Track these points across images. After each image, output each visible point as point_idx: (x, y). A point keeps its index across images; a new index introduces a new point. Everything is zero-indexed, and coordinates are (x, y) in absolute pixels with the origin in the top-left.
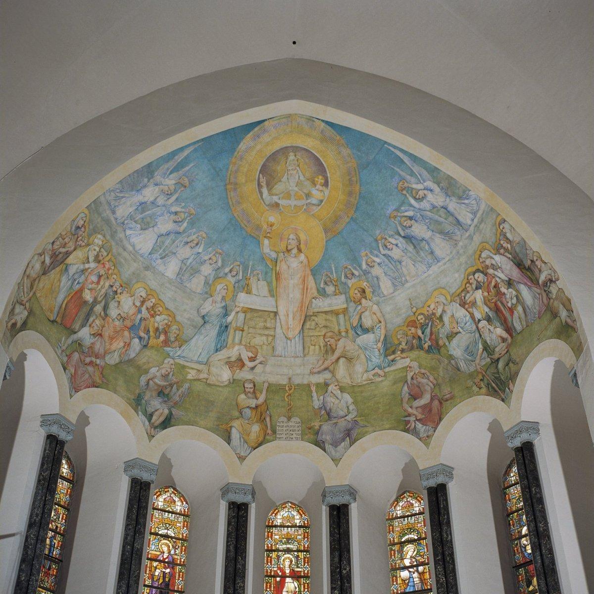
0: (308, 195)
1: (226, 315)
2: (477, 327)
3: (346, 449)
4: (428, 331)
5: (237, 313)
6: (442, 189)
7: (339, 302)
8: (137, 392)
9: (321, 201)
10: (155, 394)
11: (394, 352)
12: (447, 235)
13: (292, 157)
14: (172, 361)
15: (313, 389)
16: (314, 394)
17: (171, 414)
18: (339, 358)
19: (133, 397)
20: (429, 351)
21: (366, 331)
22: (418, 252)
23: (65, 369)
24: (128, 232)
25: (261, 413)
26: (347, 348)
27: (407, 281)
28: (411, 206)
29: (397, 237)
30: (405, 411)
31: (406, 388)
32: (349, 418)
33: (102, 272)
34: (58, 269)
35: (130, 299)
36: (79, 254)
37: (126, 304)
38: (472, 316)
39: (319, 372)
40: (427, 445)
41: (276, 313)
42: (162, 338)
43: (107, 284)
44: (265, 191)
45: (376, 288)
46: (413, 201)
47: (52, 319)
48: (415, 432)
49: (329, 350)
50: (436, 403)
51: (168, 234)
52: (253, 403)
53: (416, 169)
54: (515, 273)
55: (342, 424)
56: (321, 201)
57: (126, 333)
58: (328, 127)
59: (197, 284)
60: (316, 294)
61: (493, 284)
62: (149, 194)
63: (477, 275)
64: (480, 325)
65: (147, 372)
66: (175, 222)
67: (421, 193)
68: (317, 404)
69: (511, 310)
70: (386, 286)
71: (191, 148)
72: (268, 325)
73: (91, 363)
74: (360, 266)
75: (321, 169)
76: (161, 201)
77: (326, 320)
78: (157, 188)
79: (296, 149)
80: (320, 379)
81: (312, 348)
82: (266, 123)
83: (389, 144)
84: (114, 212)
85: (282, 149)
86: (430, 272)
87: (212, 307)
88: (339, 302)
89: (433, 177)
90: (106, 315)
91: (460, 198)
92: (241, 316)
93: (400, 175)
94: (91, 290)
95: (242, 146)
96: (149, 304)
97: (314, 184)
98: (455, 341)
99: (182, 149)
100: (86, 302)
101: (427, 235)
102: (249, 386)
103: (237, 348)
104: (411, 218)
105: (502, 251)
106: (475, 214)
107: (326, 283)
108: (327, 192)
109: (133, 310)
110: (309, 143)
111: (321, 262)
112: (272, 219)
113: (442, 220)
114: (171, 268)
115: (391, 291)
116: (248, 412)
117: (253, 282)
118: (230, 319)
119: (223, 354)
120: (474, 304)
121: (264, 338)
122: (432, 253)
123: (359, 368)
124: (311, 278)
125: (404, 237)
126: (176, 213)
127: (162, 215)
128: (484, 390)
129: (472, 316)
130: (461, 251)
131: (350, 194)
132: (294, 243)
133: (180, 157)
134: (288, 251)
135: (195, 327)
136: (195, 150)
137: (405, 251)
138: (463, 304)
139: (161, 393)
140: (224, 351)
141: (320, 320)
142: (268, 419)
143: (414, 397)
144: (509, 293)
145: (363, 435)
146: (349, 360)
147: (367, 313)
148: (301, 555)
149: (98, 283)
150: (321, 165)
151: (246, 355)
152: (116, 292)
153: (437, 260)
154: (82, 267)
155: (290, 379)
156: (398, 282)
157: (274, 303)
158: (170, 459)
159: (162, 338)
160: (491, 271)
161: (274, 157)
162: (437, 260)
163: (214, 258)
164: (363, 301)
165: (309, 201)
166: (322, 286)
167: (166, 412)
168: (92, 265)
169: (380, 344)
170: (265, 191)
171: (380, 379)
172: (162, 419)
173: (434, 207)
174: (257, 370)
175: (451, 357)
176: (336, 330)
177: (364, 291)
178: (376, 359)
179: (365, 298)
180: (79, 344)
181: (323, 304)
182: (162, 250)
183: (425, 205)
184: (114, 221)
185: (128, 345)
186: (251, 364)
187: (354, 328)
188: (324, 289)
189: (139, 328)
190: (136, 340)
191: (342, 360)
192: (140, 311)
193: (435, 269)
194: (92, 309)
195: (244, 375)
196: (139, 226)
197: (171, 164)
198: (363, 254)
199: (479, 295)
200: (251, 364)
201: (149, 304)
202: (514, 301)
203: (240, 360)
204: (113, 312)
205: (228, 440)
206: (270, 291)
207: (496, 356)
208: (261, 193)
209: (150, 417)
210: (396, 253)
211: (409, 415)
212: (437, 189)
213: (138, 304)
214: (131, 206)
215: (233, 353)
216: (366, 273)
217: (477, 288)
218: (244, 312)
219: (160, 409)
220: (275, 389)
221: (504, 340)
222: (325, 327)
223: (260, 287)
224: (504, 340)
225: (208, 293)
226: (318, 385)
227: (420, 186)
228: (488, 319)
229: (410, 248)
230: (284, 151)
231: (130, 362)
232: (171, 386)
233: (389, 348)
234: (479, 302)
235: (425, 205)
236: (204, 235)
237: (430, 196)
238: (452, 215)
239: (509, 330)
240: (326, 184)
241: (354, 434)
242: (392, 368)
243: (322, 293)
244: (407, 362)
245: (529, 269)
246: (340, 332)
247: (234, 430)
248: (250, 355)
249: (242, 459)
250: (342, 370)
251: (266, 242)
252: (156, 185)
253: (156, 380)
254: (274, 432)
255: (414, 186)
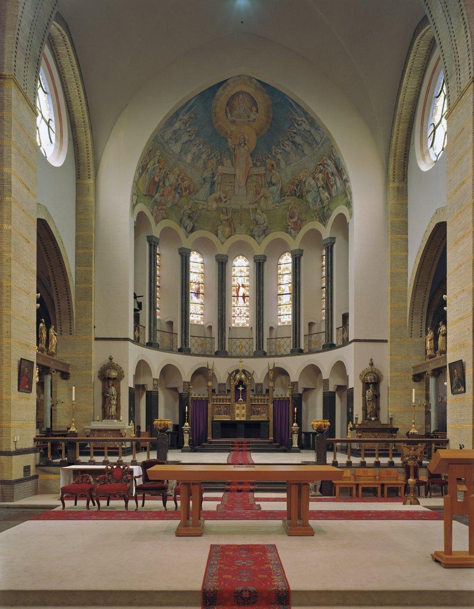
0: (249, 117)
1: (213, 177)
2: (318, 190)
3: (263, 239)
4: (299, 188)
5: (218, 176)
6: (309, 122)
7: (262, 170)
8: (180, 218)
9: (255, 120)
10: (187, 217)
11: (284, 196)
12: (310, 145)
13: (241, 96)
14: (192, 202)
15: (251, 211)
16: (251, 213)
17: (194, 225)
18: (261, 198)
19: (178, 220)
20: (299, 197)
21: (273, 185)
22: (297, 150)
23: (152, 214)
24: (170, 145)
25: (230, 223)
26: (265, 192)
27: (291, 163)
28: (295, 127)
29: (288, 141)
30: (287, 223)
31: (288, 213)
32: (265, 224)
33: (161, 167)
34: (145, 172)
35: (173, 176)
36: (152, 162)
37: (172, 178)
38: (317, 185)
39: (253, 203)
40: (294, 240)
41: (235, 175)
42: (188, 191)
43: (164, 171)
44: (229, 115)
45: (278, 165)
46: (296, 125)
47: (145, 194)
48: (290, 233)
49: (257, 193)
50: (299, 221)
51: (187, 142)
52: (226, 218)
53: (298, 110)
54: (335, 171)
55: (262, 227)
56: (255, 120)
57: (173, 192)
58: (259, 83)
59: (200, 164)
60: (252, 166)
61: (326, 172)
62: (177, 125)
63: (320, 166)
64: (320, 189)
65: (183, 208)
66: (189, 136)
67: (300, 122)
68: (252, 218)
69: (332, 186)
70: (283, 164)
71: (195, 99)
72: (232, 181)
73: (161, 209)
74: (272, 153)
75: (255, 103)
76: (182, 128)
77: (257, 178)
78: (181, 122)
79: (243, 93)
80: (254, 206)
81: (250, 192)
82: (229, 80)
83: (287, 96)
84: (163, 138)
85: (236, 93)
86: (302, 160)
87: (207, 174)
88: (262, 170)
89: (306, 116)
90: (164, 186)
91: (316, 129)
92: (220, 176)
93: (291, 112)
94: (157, 176)
95: (218, 94)
96: (181, 177)
97: (252, 111)
98: (309, 194)
99: (190, 101)
100: (156, 182)
101: (302, 142)
102: (224, 210)
103: (219, 192)
104: (295, 133)
105: (331, 159)
106: (322, 138)
107: (256, 161)
108: (257, 115)
109: (175, 181)
110: (250, 90)
111: (255, 149)
112: (232, 129)
113: (308, 136)
114: (189, 158)
115: (284, 167)
116: (224, 222)
117: (225, 159)
118: (215, 179)
119: (213, 196)
120: (318, 179)
121: (230, 187)
122: (303, 151)
123: (270, 202)
124: (250, 159)
125: (291, 142)
126: (189, 132)
127: (184, 134)
128: (318, 219)
129: (317, 185)
130: (315, 153)
131: (268, 117)
132: (242, 140)
133: (189, 105)
134: (240, 144)
135: (201, 184)
136: (197, 99)
137: (291, 148)
138: (314, 178)
139: (189, 217)
140: (214, 195)
141: (254, 178)
142: (232, 225)
143: (291, 217)
144: (332, 178)
145: (271, 232)
146: (266, 198)
147: (274, 176)
148: (246, 278)
149: (160, 172)
150: (255, 101)
151: (222, 196)
152: (167, 174)
153: (305, 155)
154: (153, 168)
155: (241, 206)
156: (288, 163)
157: (233, 170)
158: (435, 552)
159: (188, 191)
160: (326, 166)
161: (233, 98)
162: (305, 155)
163: (207, 151)
164: (273, 170)
165: (249, 119)
166: (255, 161)
167: (192, 225)
168: (157, 165)
169: (279, 192)
170: (229, 115)
171: (278, 208)
172: (191, 229)
173: (305, 130)
174: (227, 203)
175: (307, 201)
176: (261, 184)
177: (273, 166)
178: (277, 198)
179: (274, 169)
180: (156, 201)
181: (255, 171)
182: (184, 151)
183: (301, 128)
184: (164, 142)
185: (174, 197)
186: (225, 200)
187: (268, 183)
188: (256, 163)
189: (178, 189)
190: (177, 194)
191: (263, 198)
192: (177, 181)
193: (304, 159)
194: (159, 184)
195: (222, 205)
196: (174, 141)
197: (187, 108)
198: (273, 147)
199: (320, 176)
200: (225, 200)
201: (181, 177)
202: (333, 182)
203: (220, 198)
204: (167, 184)
205: (217, 235)
206: (232, 164)
207: (324, 205)
208: (227, 116)
209: (186, 228)
210: (288, 149)
211: (289, 225)
212: (307, 122)
213: (177, 177)
214: (170, 133)
215: (217, 194)
216: (274, 157)
217: (320, 172)
218: (221, 175)
219: (190, 224)
220: (235, 211)
221: (328, 199)
222: (256, 182)
223: (227, 162)
224: (328, 199)
225: (205, 167)
226: (253, 209)
227: (299, 119)
228: (323, 187)
229: (294, 148)
230: (237, 94)
231: (176, 205)
232: (193, 213)
233: (282, 194)
234: (320, 179)
235: (301, 128)
236: (202, 140)
237: (304, 125)
238: (313, 136)
239: (330, 194)
240: (257, 111)
241: (267, 233)
242: (283, 203)
243: (255, 165)
244: (290, 201)
245: (340, 171)
246: (262, 185)
247: (219, 231)
248: (225, 195)
249: (223, 243)
250: (262, 203)
251: (230, 140)
252: (180, 120)
253: (187, 211)
254: (235, 230)
255: (297, 118)
